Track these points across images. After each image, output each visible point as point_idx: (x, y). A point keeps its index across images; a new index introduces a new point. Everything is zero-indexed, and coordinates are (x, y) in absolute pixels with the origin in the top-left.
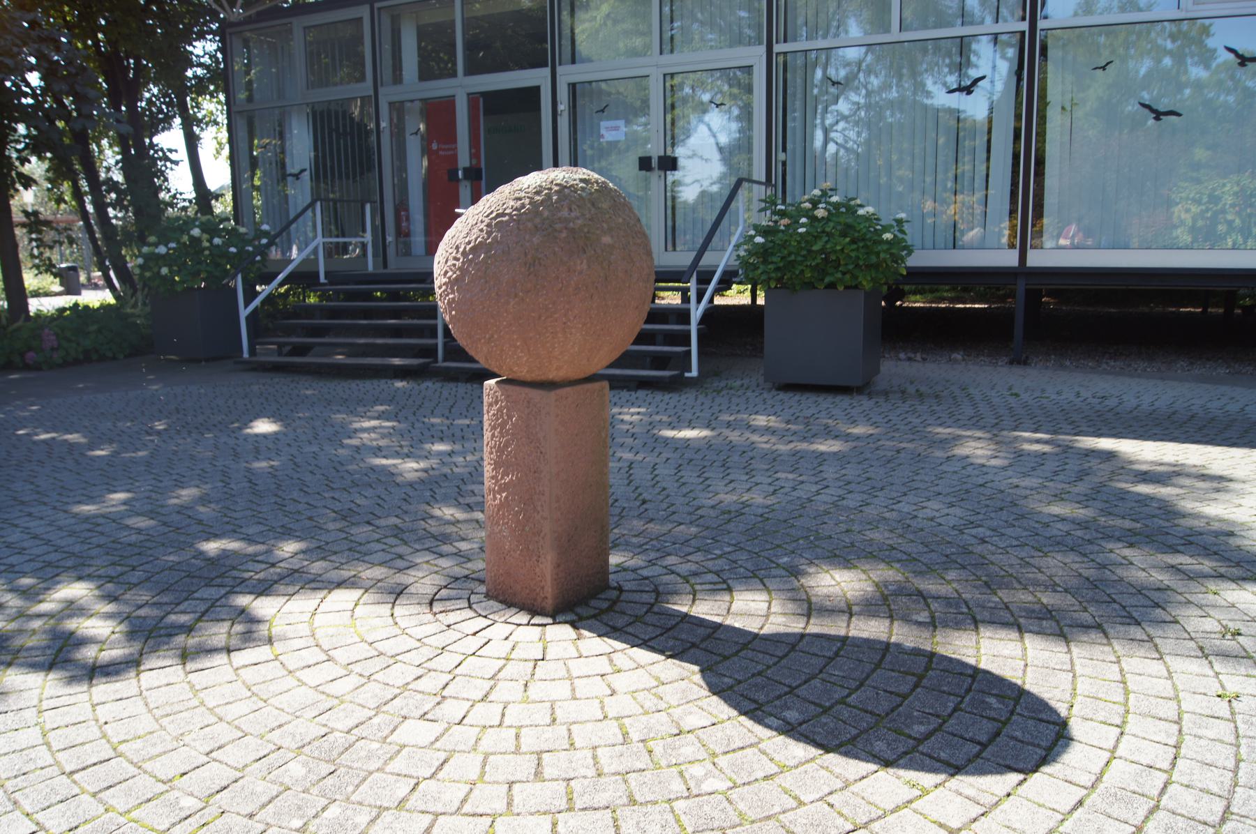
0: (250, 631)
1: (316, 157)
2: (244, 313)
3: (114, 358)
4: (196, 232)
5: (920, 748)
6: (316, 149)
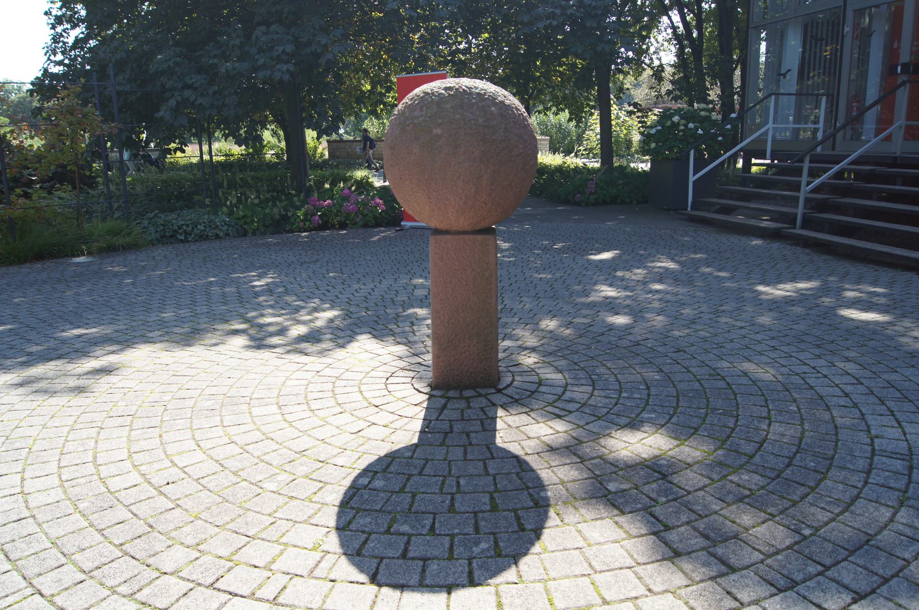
0: (32, 84)
1: (803, 52)
2: (692, 179)
3: (631, 203)
4: (676, 119)
5: (827, 573)
6: (804, 47)
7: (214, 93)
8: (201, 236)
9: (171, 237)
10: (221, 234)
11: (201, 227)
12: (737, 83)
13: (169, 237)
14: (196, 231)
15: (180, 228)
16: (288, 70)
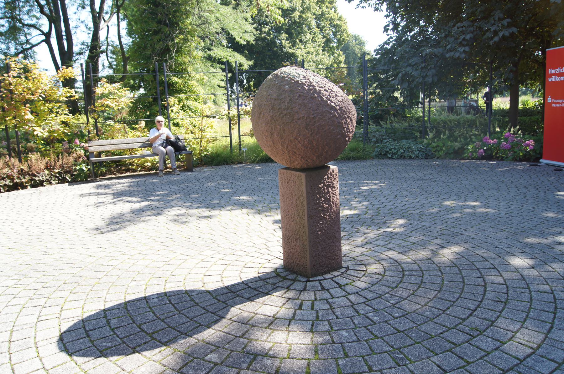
7: (422, 68)
8: (401, 156)
9: (385, 155)
10: (413, 156)
11: (402, 151)
12: (151, 172)
13: (383, 155)
14: (399, 153)
15: (390, 150)
16: (464, 51)
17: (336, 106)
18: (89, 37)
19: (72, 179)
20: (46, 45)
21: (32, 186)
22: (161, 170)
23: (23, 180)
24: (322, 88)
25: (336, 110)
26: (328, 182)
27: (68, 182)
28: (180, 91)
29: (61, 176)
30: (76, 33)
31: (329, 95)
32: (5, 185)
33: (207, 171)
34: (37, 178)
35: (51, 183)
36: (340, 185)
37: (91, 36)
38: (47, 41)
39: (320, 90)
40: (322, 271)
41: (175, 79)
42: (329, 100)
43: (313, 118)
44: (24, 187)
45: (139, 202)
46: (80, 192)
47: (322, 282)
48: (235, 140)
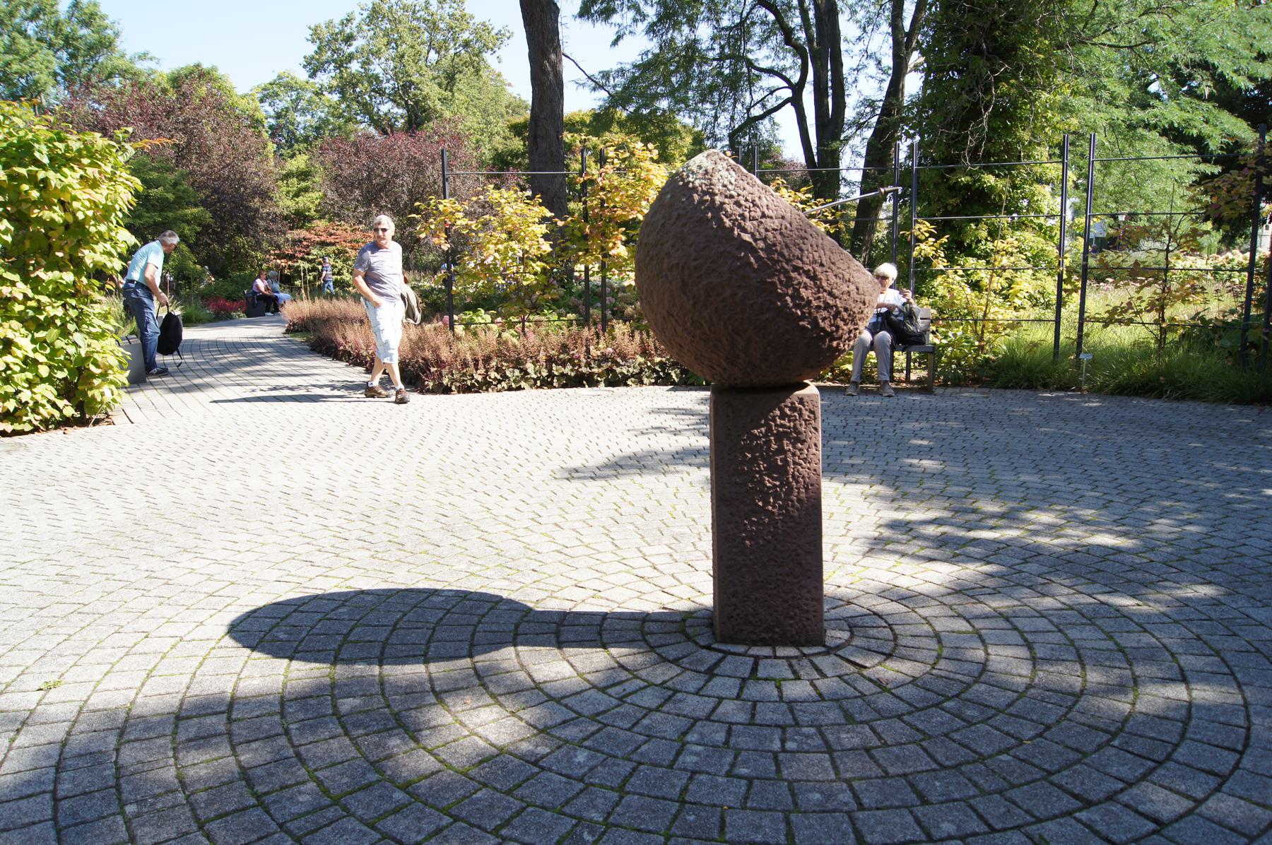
17: (756, 240)
18: (880, 89)
19: (681, 379)
20: (792, 109)
21: (610, 383)
22: (855, 383)
23: (596, 370)
24: (731, 197)
25: (754, 251)
26: (783, 426)
27: (673, 383)
28: (995, 208)
29: (663, 371)
30: (856, 81)
31: (742, 215)
32: (562, 375)
33: (969, 396)
34: (618, 370)
35: (641, 383)
36: (828, 437)
37: (886, 85)
38: (796, 101)
39: (722, 203)
40: (754, 637)
41: (990, 179)
42: (740, 226)
43: (696, 268)
44: (593, 383)
45: (676, 433)
46: (648, 404)
47: (794, 662)
48: (1068, 333)
